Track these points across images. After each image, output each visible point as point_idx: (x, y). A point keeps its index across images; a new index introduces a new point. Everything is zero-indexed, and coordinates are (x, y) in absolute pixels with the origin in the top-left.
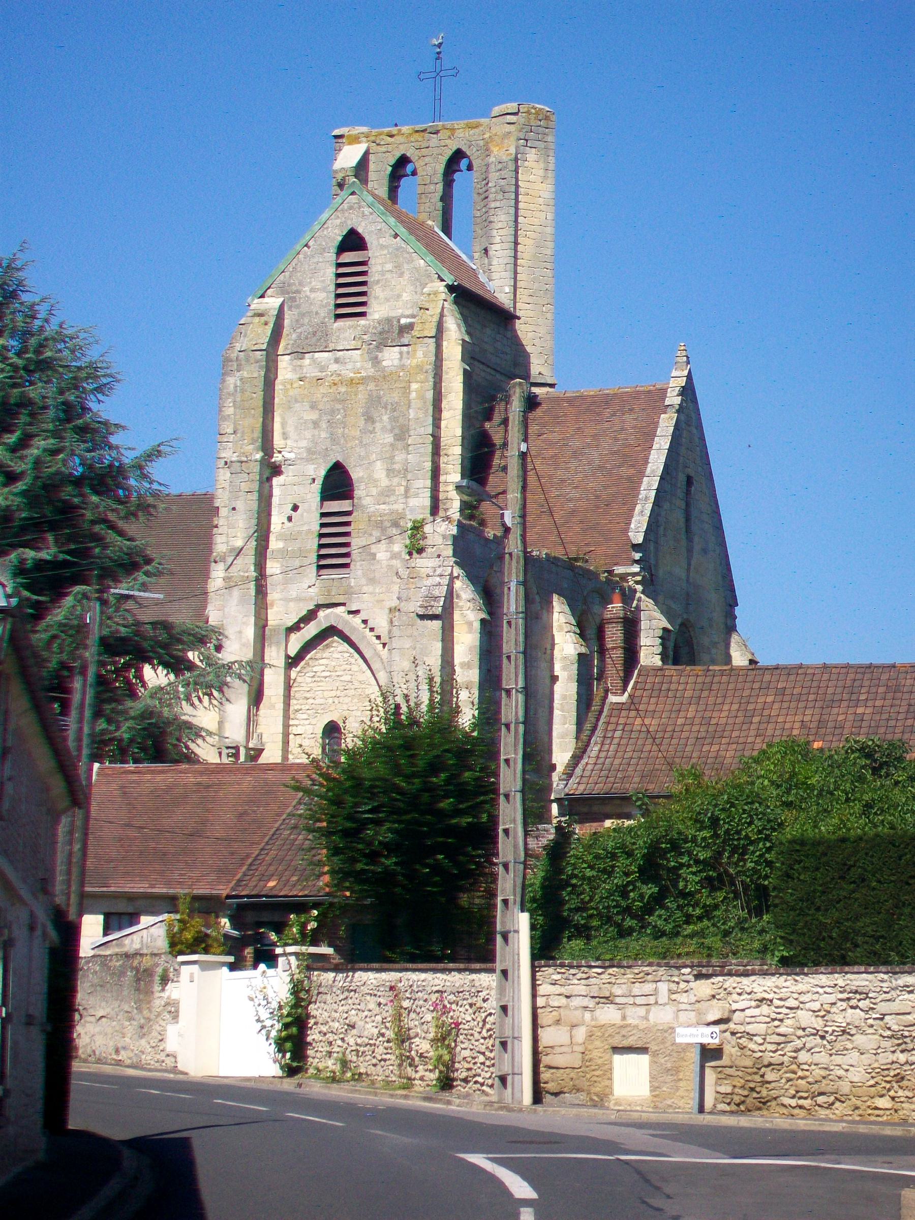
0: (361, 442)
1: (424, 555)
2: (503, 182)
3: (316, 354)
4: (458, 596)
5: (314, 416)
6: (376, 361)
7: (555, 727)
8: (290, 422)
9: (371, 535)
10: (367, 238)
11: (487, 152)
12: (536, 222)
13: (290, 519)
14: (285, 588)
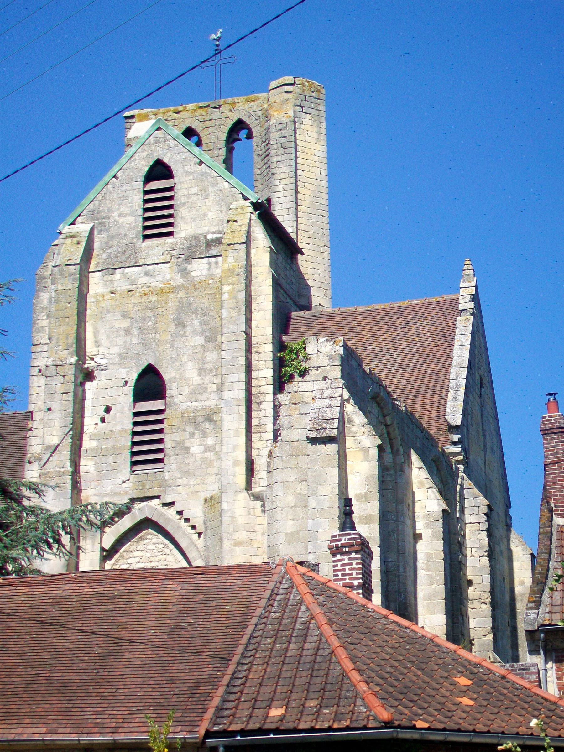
0: (172, 345)
1: (307, 377)
2: (283, 140)
3: (127, 270)
4: (350, 421)
5: (126, 324)
6: (184, 272)
7: (419, 588)
8: (102, 331)
9: (184, 430)
10: (173, 167)
11: (267, 117)
12: (312, 176)
13: (103, 420)
14: (99, 484)
